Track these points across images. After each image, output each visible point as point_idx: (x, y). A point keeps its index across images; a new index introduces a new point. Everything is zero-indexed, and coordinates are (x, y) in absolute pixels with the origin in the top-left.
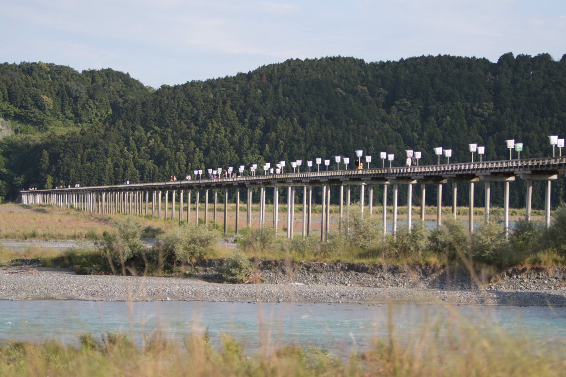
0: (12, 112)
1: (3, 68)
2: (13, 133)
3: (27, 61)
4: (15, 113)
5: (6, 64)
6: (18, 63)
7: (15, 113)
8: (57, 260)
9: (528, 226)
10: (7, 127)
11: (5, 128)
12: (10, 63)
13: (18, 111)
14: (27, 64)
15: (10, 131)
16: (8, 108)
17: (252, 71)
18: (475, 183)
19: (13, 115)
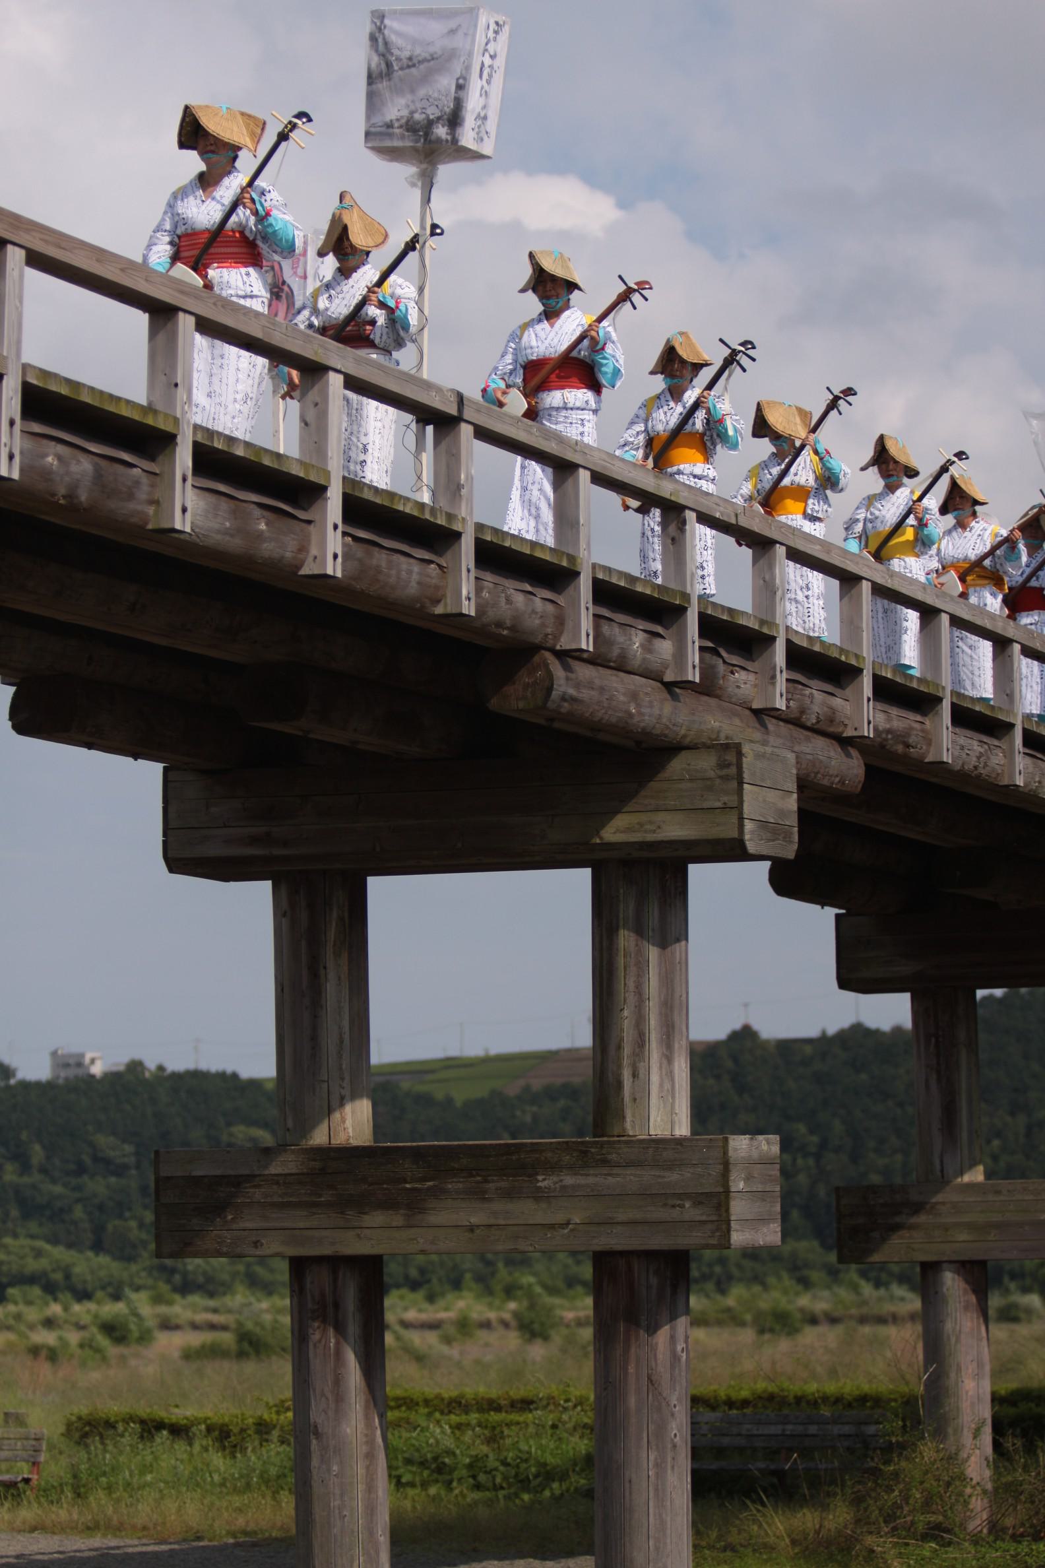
5: (135, 1067)
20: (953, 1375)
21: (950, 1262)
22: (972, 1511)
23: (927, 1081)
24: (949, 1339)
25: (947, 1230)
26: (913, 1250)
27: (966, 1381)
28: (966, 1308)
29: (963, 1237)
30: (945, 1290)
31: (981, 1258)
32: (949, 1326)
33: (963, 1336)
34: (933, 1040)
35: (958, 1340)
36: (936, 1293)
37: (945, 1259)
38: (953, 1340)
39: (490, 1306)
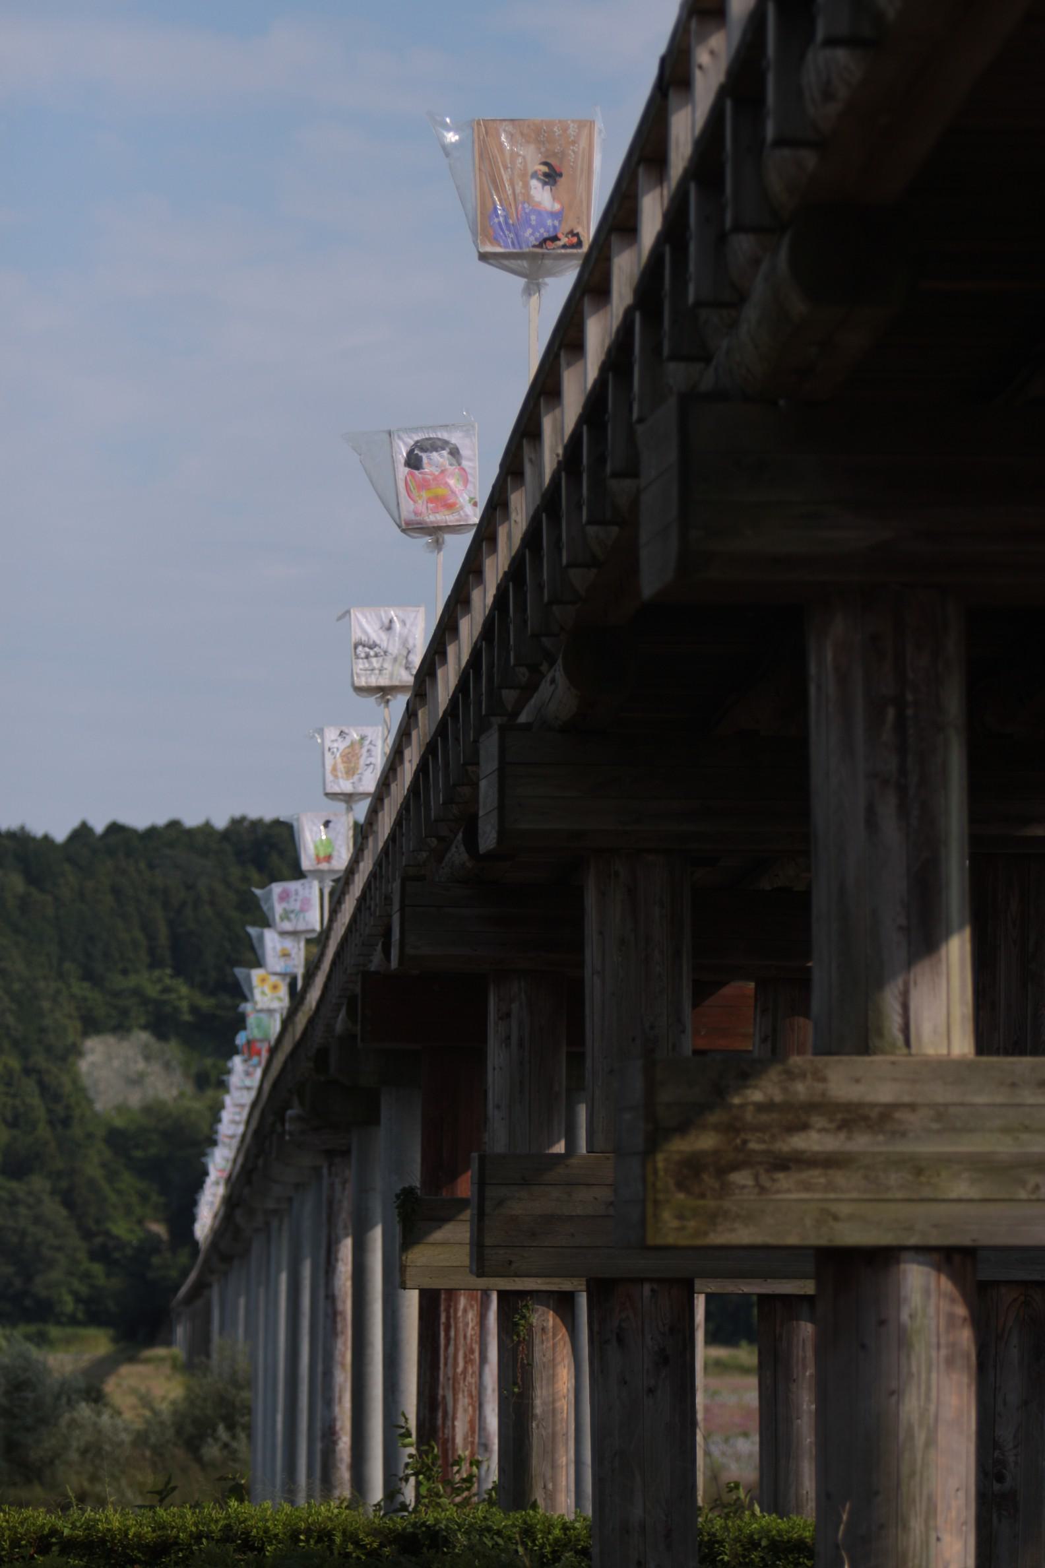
0: (184, 1005)
1: (18, 850)
2: (189, 1089)
3: (253, 815)
4: (194, 1009)
5: (174, 825)
6: (221, 823)
7: (194, 1009)
8: (828, 1496)
9: (557, 1532)
10: (167, 1066)
11: (156, 1067)
12: (191, 821)
13: (206, 1003)
14: (257, 824)
15: (178, 1076)
16: (166, 990)
17: (99, 827)
18: (709, 1298)
19: (187, 1017)
20: (916, 1525)
21: (923, 1251)
22: (147, 1422)
23: (870, 810)
24: (911, 1437)
25: (919, 1171)
26: (836, 1218)
27: (947, 1538)
28: (950, 1362)
29: (962, 1188)
30: (905, 1316)
31: (966, 1241)
32: (911, 1407)
33: (942, 1430)
34: (891, 713)
35: (931, 1442)
36: (882, 1323)
37: (913, 1241)
38: (920, 1438)
39: (90, 1527)
